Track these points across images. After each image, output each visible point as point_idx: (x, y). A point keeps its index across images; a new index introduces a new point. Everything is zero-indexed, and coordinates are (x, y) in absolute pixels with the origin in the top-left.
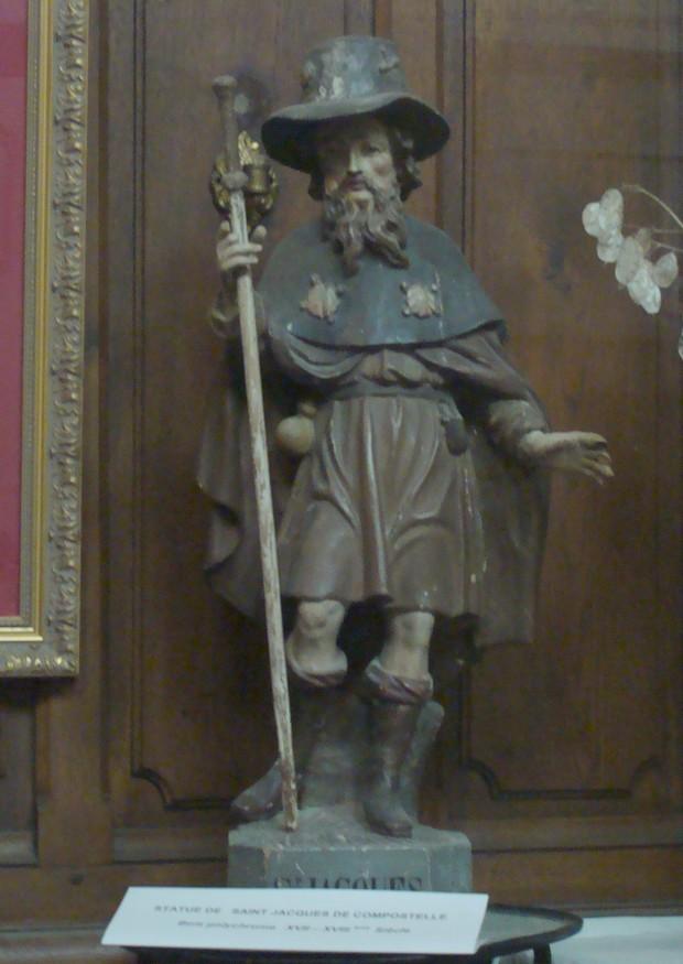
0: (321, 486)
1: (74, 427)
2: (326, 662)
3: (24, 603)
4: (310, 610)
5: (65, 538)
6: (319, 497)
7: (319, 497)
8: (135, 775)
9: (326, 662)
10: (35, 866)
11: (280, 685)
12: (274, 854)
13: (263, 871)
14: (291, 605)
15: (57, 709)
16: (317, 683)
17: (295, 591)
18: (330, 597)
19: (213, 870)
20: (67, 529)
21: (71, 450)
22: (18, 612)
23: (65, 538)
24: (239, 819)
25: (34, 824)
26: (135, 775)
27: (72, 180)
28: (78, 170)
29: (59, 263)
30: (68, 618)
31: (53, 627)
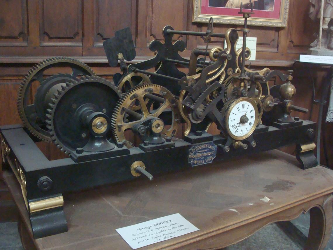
0: (329, 2)
1: (287, 16)
2: (326, 27)
3: (280, 17)
4: (326, 19)
5: (286, 8)
6: (329, 4)
7: (329, 4)
8: (290, 41)
9: (326, 27)
10: (278, 52)
11: (321, 29)
12: (319, 52)
13: (317, 54)
14: (324, 18)
15: (282, 32)
16: (325, 29)
17: (324, 17)
18: (330, 18)
19: (310, 53)
20: (287, 7)
21: (287, 8)
22: (279, 18)
23: (286, 8)
24: (311, 47)
25: (278, 47)
26: (290, 41)
27: (286, 17)
28: (287, 15)
29: (286, 5)
30: (286, 19)
31: (284, 20)
